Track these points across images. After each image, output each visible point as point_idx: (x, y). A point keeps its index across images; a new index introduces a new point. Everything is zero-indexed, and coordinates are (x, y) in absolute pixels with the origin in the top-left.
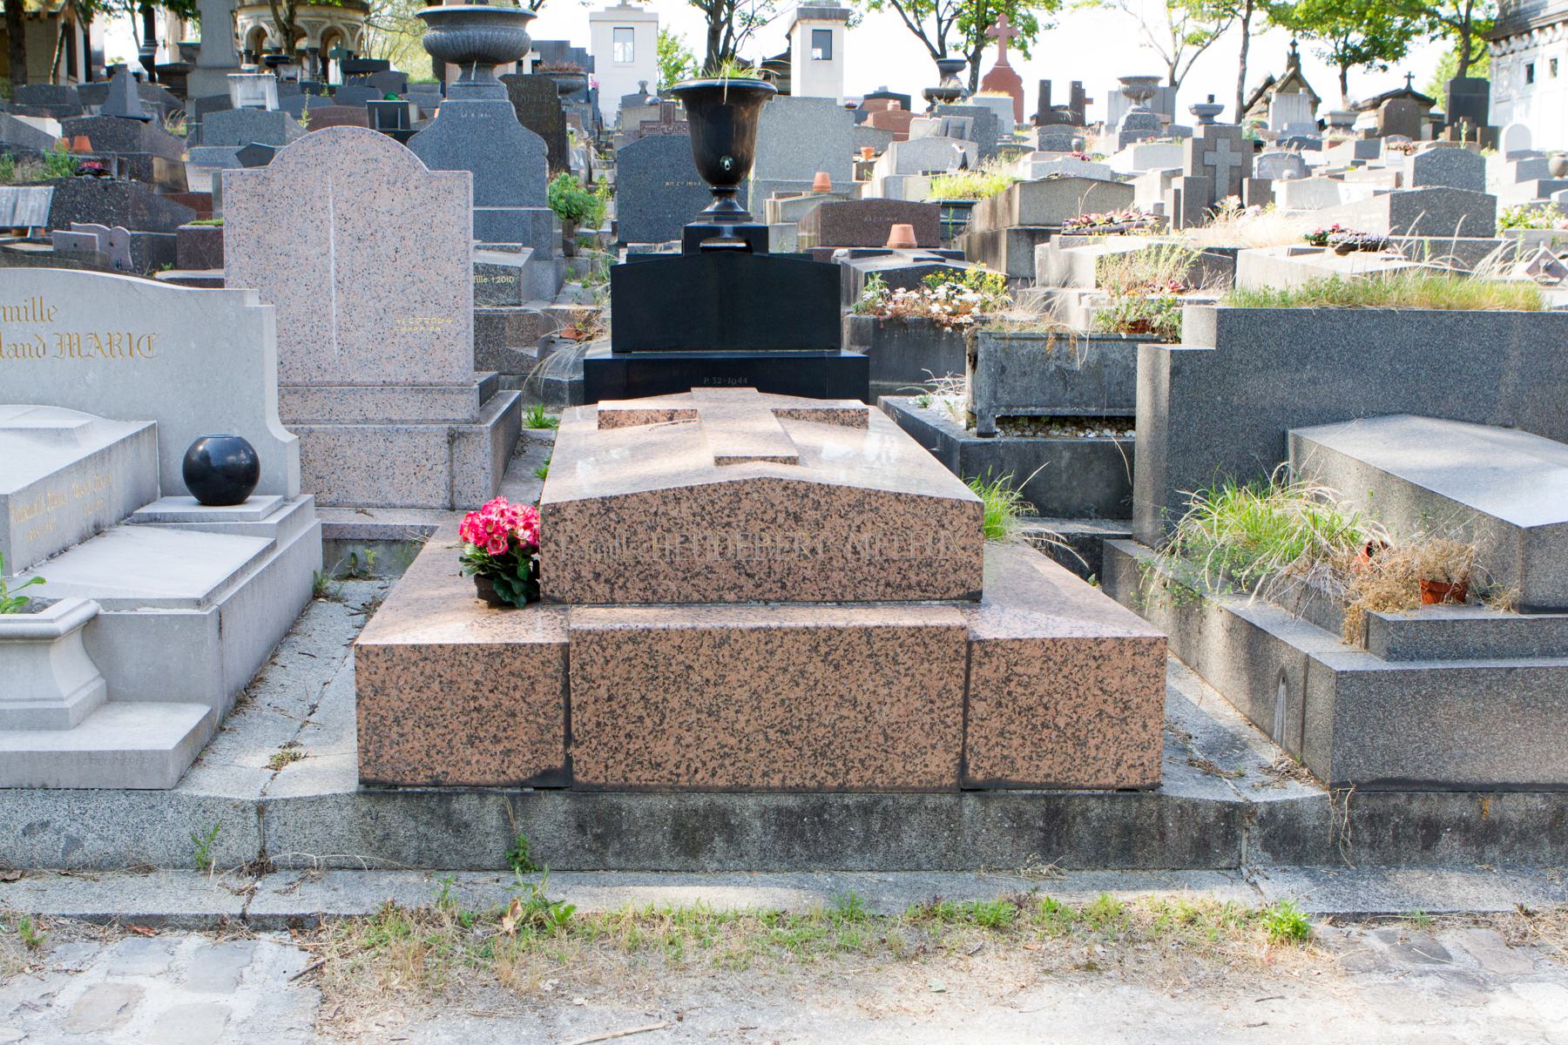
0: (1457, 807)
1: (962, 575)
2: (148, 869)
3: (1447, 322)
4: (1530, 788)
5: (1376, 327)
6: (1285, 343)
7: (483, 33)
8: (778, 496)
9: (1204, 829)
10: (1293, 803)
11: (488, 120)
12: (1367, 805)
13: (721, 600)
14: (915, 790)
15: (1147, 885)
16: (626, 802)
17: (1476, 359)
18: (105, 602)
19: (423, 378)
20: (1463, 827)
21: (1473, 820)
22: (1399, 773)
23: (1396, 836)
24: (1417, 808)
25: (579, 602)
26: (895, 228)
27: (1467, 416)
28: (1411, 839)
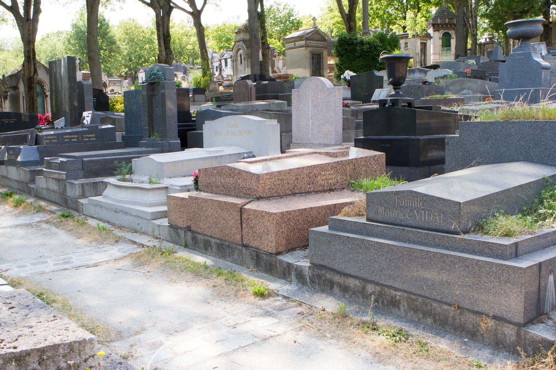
0: (337, 278)
1: (255, 193)
2: (136, 232)
3: (540, 125)
4: (356, 277)
5: (512, 128)
6: (481, 134)
7: (531, 28)
8: (228, 170)
9: (284, 268)
10: (301, 266)
11: (523, 59)
12: (317, 272)
13: (221, 194)
14: (235, 244)
15: (263, 278)
16: (198, 236)
17: (552, 140)
18: (171, 185)
19: (326, 143)
20: (339, 285)
21: (342, 284)
22: (324, 264)
23: (324, 283)
24: (328, 276)
25: (203, 191)
26: (85, 114)
27: (550, 163)
28: (327, 285)
